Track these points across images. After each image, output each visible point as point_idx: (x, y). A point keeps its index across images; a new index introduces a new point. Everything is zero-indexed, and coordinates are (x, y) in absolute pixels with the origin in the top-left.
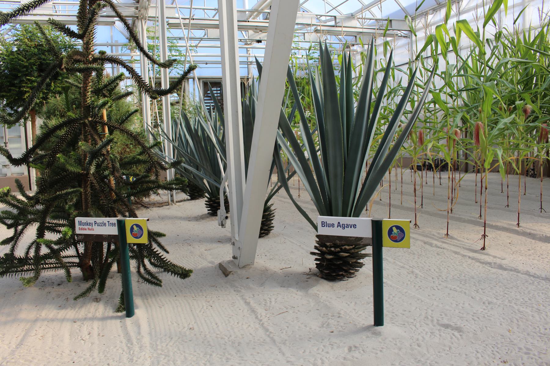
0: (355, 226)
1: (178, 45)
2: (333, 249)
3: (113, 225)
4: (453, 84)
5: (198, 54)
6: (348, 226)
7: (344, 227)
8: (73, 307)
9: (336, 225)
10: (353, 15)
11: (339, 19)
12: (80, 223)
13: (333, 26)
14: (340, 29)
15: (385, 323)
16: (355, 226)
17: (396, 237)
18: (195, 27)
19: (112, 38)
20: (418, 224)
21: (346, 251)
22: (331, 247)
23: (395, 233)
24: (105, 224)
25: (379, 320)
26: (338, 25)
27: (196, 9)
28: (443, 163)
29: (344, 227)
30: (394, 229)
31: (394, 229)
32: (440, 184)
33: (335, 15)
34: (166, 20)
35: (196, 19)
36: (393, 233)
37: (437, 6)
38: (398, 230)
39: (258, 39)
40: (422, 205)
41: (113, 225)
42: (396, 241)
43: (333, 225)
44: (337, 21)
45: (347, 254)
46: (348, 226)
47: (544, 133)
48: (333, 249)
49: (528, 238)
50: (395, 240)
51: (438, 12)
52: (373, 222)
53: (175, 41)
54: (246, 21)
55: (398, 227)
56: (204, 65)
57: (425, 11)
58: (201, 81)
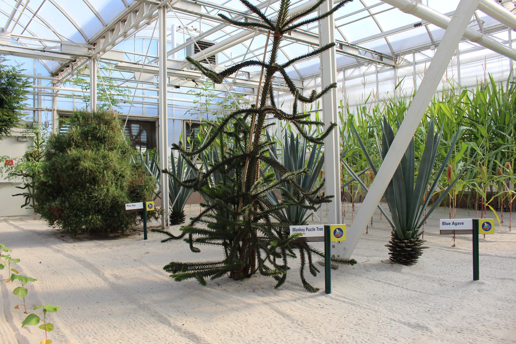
0: (463, 223)
2: (409, 244)
3: (321, 229)
4: (342, 133)
6: (458, 224)
7: (456, 224)
8: (275, 294)
9: (451, 224)
11: (252, 75)
12: (294, 230)
15: (480, 278)
16: (463, 223)
17: (338, 235)
19: (35, 70)
21: (409, 247)
22: (408, 243)
24: (315, 229)
25: (476, 276)
26: (251, 80)
28: (55, 204)
29: (456, 224)
30: (485, 224)
31: (485, 224)
34: (167, 71)
35: (140, 64)
39: (177, 85)
41: (321, 229)
42: (486, 231)
43: (449, 224)
44: (251, 76)
45: (410, 249)
46: (458, 224)
48: (409, 244)
50: (486, 230)
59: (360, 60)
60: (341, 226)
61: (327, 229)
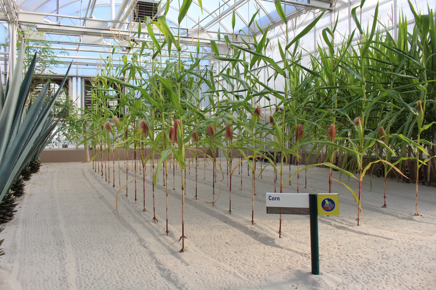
0: (278, 199)
1: (52, 47)
5: (70, 56)
10: (203, 28)
11: (190, 31)
13: (185, 37)
14: (190, 40)
17: (328, 207)
18: (58, 32)
20: (156, 218)
23: (327, 204)
26: (189, 36)
27: (63, 17)
30: (326, 201)
31: (326, 201)
32: (248, 175)
33: (187, 28)
35: (61, 26)
36: (325, 204)
37: (272, 24)
38: (330, 202)
40: (196, 196)
42: (328, 211)
47: (299, 133)
49: (252, 237)
51: (273, 29)
52: (310, 196)
53: (48, 44)
54: (107, 30)
55: (329, 200)
56: (86, 67)
57: (264, 28)
58: (83, 80)
59: (300, 8)
60: (333, 195)
61: (313, 199)
